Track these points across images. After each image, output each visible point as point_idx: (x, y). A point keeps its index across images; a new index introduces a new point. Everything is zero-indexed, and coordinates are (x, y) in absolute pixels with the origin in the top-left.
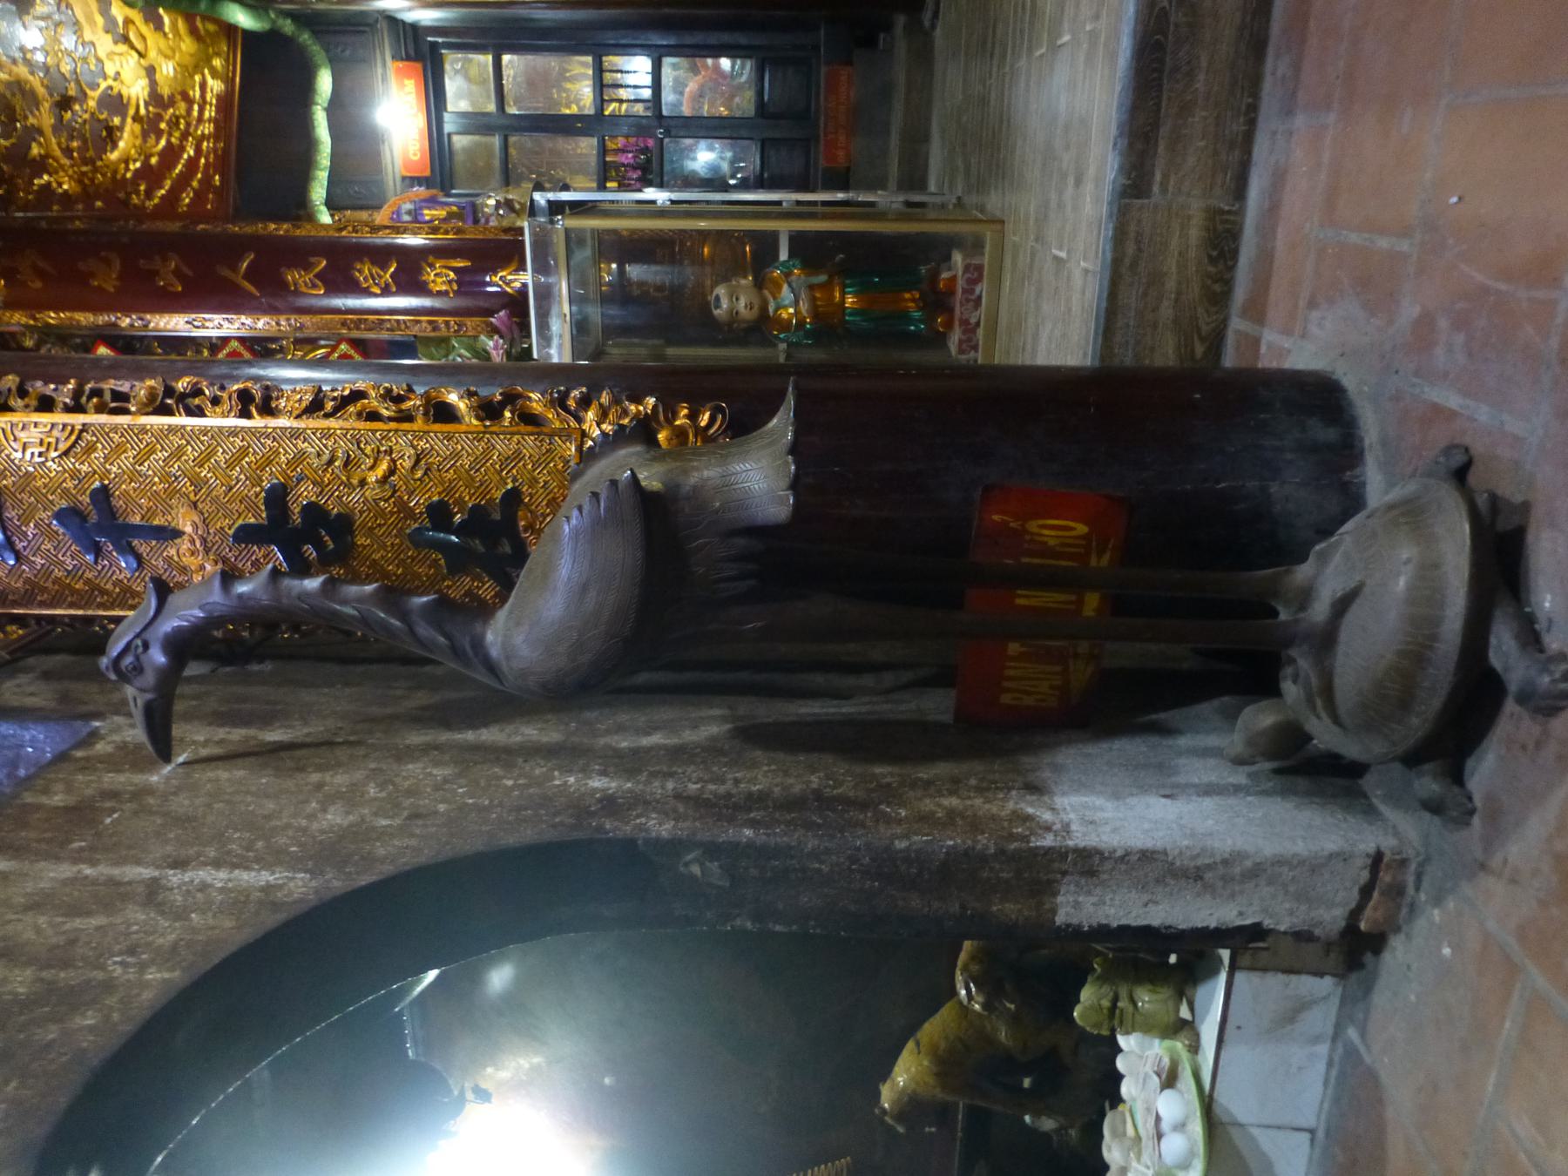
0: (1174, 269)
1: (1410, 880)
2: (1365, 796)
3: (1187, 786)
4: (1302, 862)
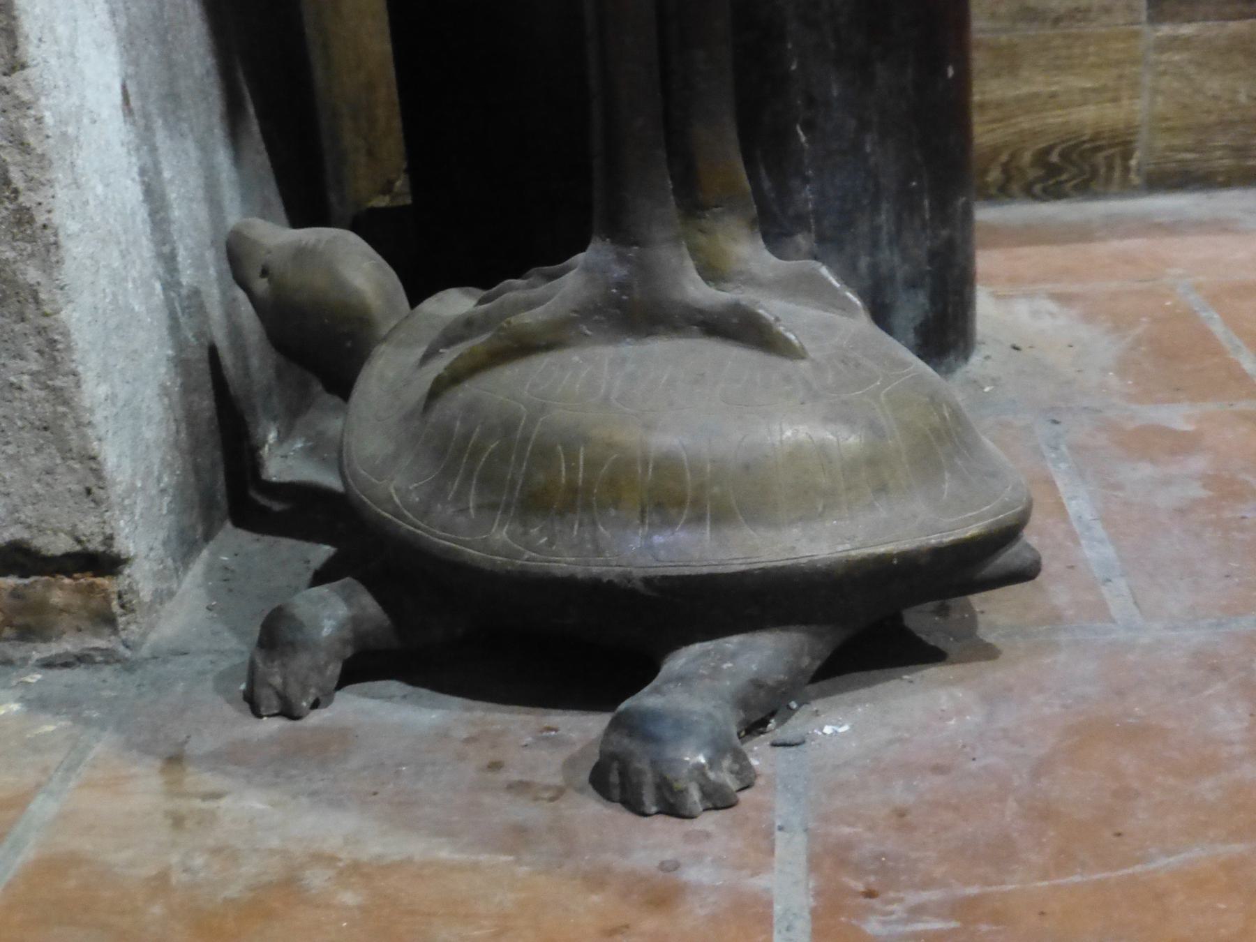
0: (1025, 90)
1: (67, 645)
2: (208, 537)
3: (153, 149)
4: (60, 396)
